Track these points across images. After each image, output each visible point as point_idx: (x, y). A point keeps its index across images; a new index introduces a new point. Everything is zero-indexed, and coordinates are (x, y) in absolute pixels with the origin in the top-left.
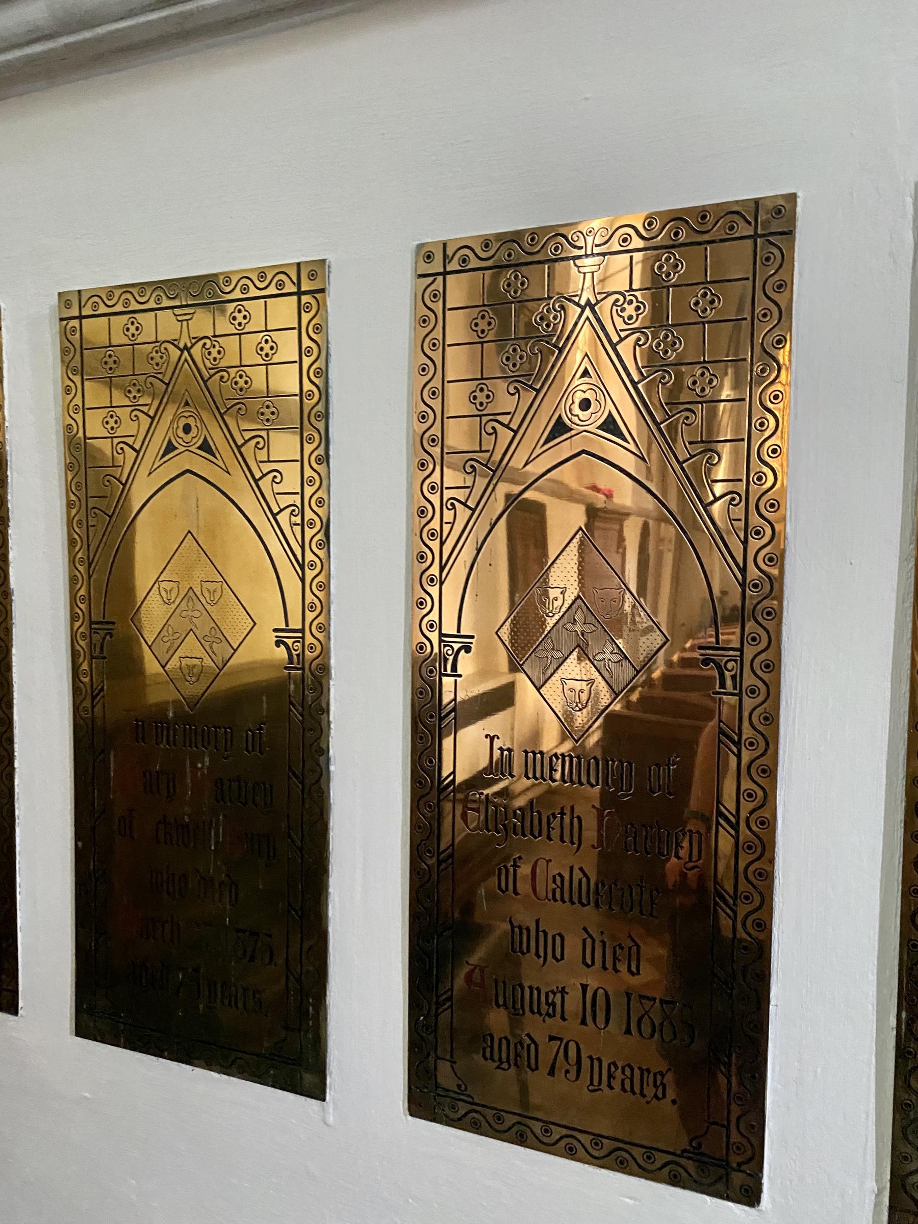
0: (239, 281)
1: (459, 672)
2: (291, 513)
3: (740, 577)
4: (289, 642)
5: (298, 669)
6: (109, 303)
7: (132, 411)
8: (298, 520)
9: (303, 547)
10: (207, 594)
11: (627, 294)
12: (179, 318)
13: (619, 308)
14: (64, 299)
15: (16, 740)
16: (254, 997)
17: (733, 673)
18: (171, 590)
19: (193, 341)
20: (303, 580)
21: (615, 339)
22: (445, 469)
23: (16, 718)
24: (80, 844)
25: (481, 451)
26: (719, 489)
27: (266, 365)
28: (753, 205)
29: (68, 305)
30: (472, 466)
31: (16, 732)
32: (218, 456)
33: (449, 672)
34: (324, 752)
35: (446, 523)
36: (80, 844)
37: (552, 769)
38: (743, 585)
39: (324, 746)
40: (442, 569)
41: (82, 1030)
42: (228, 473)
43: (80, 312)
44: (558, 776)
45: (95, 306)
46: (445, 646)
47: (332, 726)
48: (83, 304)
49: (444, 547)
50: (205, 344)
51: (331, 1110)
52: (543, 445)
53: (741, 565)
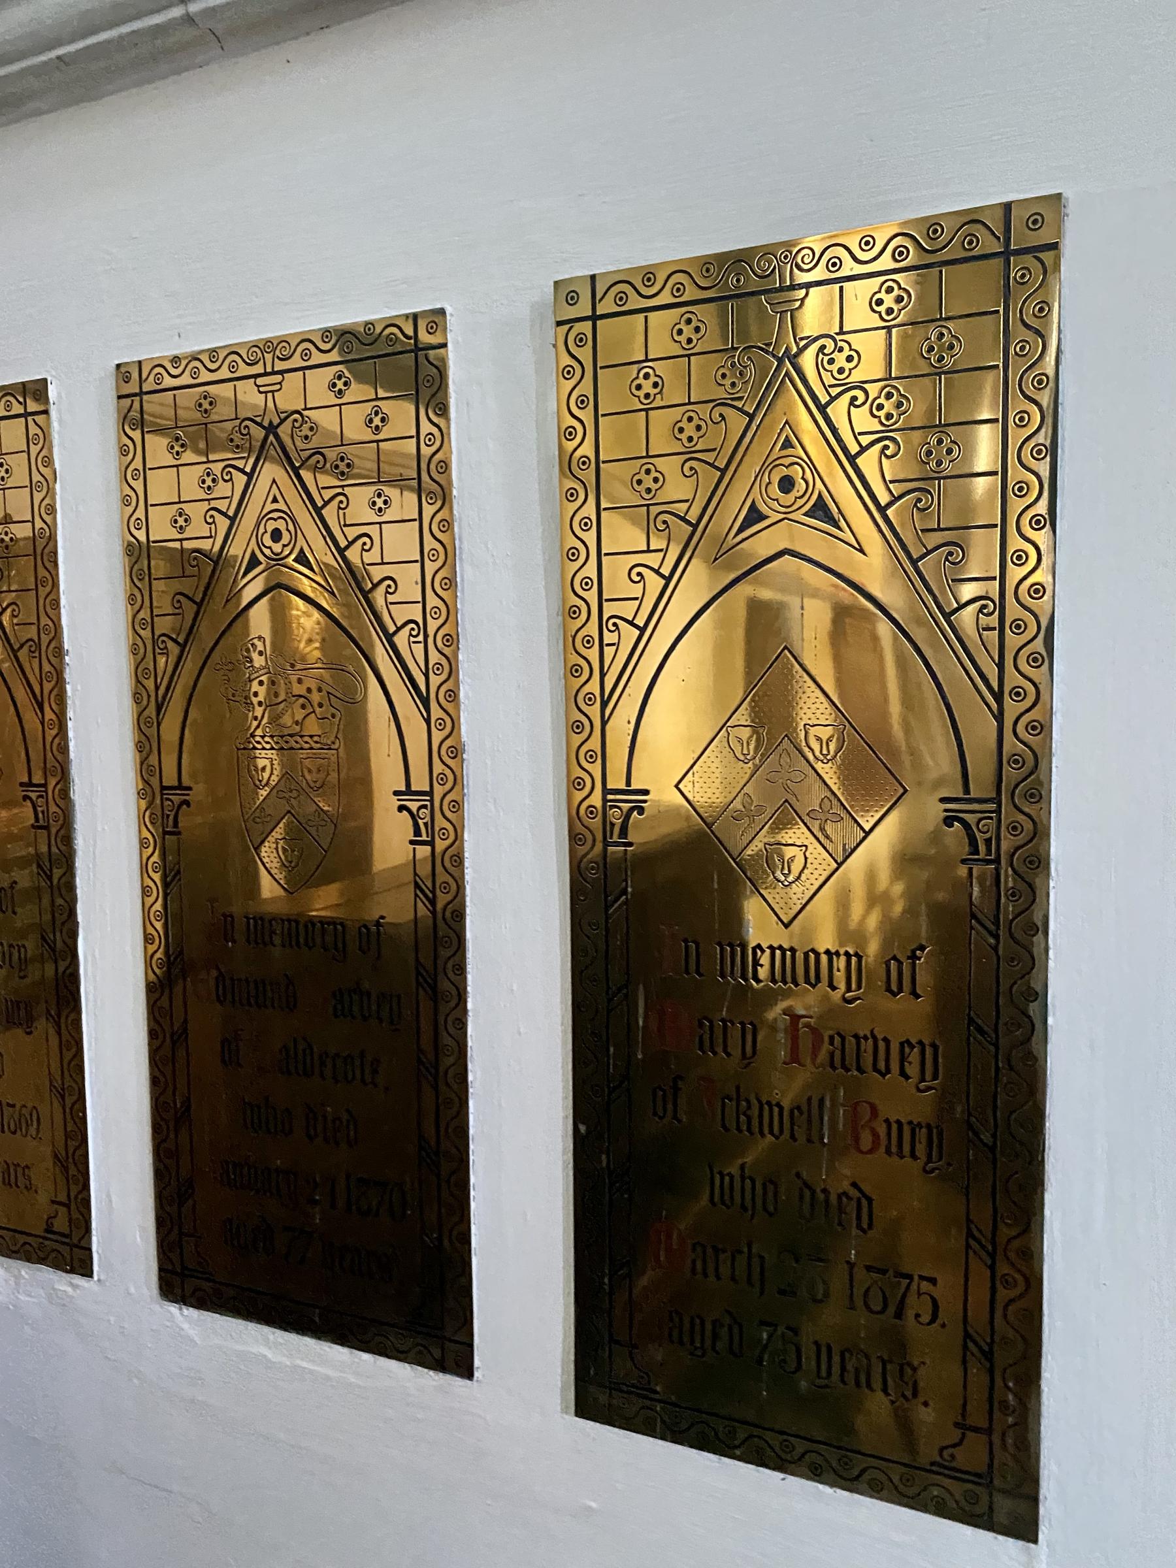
0: (298, 345)
1: (630, 839)
2: (980, 611)
3: (994, 706)
4: (971, 818)
5: (989, 862)
6: (174, 372)
7: (685, 462)
8: (994, 621)
9: (1001, 666)
10: (816, 746)
11: (838, 338)
12: (262, 389)
13: (826, 359)
14: (566, 292)
15: (469, 968)
16: (24, 1174)
17: (988, 836)
18: (829, 740)
19: (802, 343)
20: (999, 717)
21: (824, 398)
22: (265, 600)
23: (469, 935)
24: (582, 1128)
25: (648, 551)
26: (968, 591)
27: (646, 410)
28: (1000, 213)
29: (572, 298)
30: (639, 574)
31: (470, 955)
32: (843, 524)
33: (615, 838)
34: (1039, 996)
35: (608, 645)
36: (582, 1128)
37: (756, 963)
38: (42, 723)
39: (1038, 988)
40: (159, 708)
41: (587, 1406)
42: (861, 551)
43: (141, 388)
44: (763, 973)
45: (622, 298)
46: (612, 807)
47: (1051, 953)
48: (144, 376)
49: (606, 678)
50: (823, 347)
51: (1043, 1557)
52: (839, 528)
53: (996, 689)
